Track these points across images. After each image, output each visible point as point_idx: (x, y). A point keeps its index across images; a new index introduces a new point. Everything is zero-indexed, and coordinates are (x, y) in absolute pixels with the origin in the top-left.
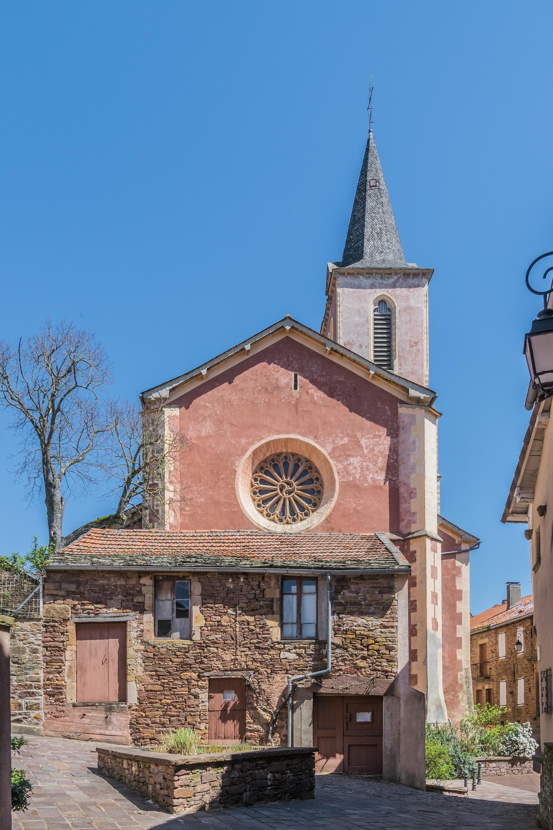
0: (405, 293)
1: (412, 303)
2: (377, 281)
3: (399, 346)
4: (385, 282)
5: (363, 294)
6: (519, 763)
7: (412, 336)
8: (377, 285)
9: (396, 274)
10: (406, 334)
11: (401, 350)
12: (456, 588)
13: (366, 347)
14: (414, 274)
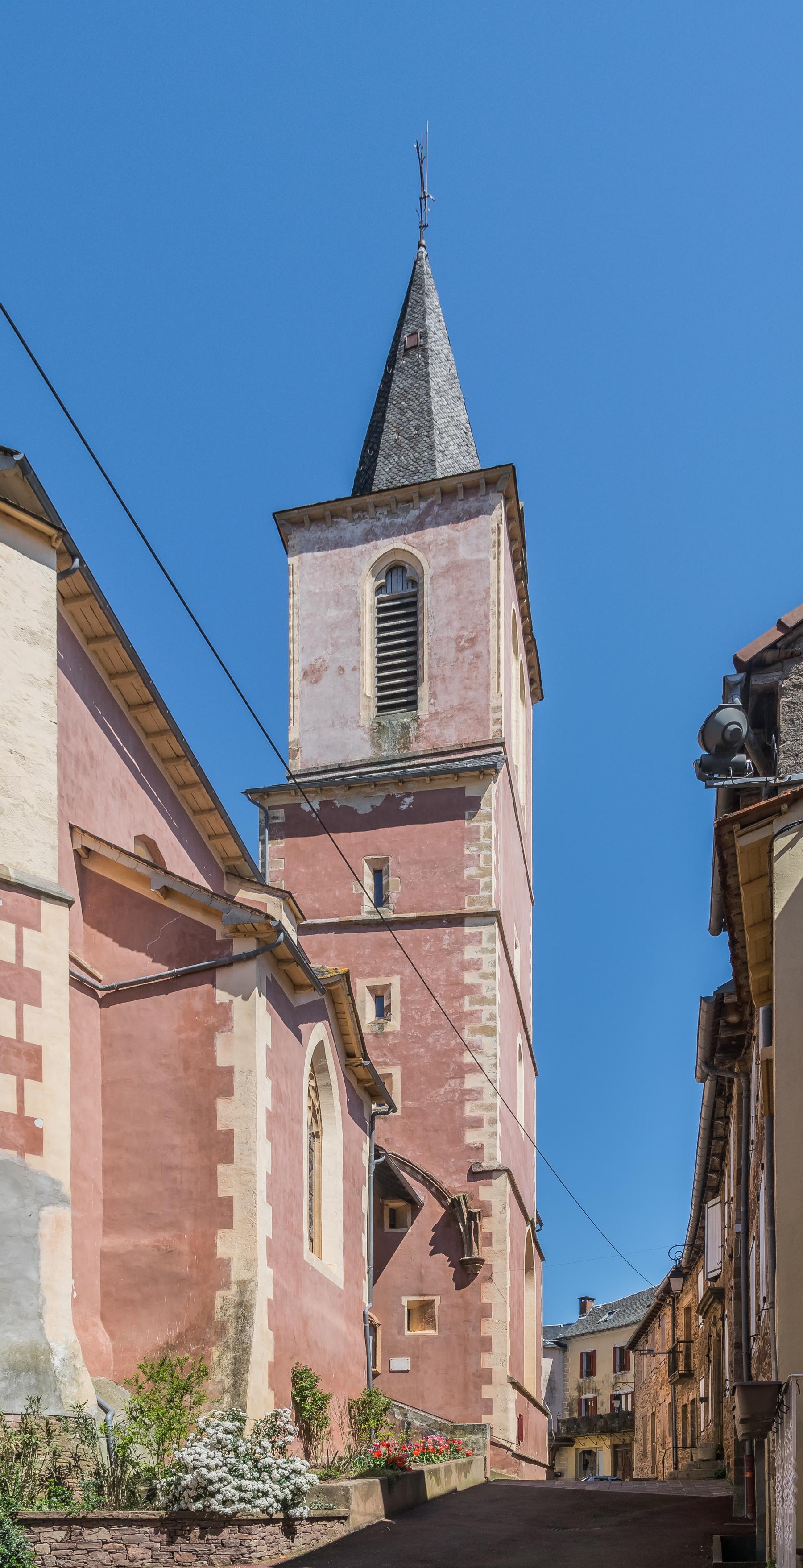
0: (446, 536)
1: (464, 553)
2: (378, 523)
3: (430, 654)
4: (399, 521)
5: (346, 557)
6: (197, 1531)
7: (463, 628)
8: (378, 531)
9: (422, 497)
10: (449, 624)
11: (434, 663)
12: (215, 1064)
13: (354, 669)
14: (466, 489)
